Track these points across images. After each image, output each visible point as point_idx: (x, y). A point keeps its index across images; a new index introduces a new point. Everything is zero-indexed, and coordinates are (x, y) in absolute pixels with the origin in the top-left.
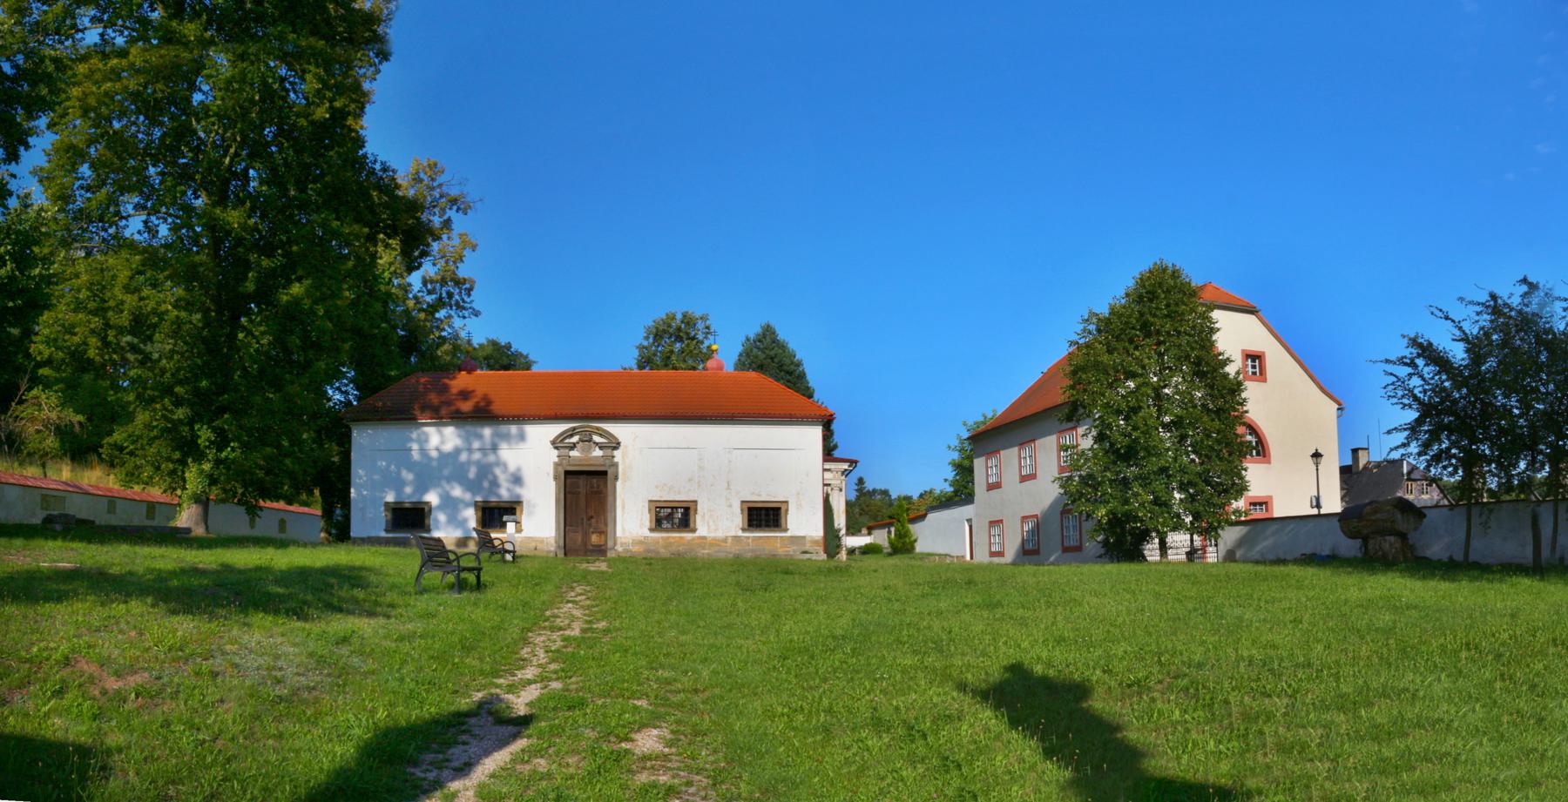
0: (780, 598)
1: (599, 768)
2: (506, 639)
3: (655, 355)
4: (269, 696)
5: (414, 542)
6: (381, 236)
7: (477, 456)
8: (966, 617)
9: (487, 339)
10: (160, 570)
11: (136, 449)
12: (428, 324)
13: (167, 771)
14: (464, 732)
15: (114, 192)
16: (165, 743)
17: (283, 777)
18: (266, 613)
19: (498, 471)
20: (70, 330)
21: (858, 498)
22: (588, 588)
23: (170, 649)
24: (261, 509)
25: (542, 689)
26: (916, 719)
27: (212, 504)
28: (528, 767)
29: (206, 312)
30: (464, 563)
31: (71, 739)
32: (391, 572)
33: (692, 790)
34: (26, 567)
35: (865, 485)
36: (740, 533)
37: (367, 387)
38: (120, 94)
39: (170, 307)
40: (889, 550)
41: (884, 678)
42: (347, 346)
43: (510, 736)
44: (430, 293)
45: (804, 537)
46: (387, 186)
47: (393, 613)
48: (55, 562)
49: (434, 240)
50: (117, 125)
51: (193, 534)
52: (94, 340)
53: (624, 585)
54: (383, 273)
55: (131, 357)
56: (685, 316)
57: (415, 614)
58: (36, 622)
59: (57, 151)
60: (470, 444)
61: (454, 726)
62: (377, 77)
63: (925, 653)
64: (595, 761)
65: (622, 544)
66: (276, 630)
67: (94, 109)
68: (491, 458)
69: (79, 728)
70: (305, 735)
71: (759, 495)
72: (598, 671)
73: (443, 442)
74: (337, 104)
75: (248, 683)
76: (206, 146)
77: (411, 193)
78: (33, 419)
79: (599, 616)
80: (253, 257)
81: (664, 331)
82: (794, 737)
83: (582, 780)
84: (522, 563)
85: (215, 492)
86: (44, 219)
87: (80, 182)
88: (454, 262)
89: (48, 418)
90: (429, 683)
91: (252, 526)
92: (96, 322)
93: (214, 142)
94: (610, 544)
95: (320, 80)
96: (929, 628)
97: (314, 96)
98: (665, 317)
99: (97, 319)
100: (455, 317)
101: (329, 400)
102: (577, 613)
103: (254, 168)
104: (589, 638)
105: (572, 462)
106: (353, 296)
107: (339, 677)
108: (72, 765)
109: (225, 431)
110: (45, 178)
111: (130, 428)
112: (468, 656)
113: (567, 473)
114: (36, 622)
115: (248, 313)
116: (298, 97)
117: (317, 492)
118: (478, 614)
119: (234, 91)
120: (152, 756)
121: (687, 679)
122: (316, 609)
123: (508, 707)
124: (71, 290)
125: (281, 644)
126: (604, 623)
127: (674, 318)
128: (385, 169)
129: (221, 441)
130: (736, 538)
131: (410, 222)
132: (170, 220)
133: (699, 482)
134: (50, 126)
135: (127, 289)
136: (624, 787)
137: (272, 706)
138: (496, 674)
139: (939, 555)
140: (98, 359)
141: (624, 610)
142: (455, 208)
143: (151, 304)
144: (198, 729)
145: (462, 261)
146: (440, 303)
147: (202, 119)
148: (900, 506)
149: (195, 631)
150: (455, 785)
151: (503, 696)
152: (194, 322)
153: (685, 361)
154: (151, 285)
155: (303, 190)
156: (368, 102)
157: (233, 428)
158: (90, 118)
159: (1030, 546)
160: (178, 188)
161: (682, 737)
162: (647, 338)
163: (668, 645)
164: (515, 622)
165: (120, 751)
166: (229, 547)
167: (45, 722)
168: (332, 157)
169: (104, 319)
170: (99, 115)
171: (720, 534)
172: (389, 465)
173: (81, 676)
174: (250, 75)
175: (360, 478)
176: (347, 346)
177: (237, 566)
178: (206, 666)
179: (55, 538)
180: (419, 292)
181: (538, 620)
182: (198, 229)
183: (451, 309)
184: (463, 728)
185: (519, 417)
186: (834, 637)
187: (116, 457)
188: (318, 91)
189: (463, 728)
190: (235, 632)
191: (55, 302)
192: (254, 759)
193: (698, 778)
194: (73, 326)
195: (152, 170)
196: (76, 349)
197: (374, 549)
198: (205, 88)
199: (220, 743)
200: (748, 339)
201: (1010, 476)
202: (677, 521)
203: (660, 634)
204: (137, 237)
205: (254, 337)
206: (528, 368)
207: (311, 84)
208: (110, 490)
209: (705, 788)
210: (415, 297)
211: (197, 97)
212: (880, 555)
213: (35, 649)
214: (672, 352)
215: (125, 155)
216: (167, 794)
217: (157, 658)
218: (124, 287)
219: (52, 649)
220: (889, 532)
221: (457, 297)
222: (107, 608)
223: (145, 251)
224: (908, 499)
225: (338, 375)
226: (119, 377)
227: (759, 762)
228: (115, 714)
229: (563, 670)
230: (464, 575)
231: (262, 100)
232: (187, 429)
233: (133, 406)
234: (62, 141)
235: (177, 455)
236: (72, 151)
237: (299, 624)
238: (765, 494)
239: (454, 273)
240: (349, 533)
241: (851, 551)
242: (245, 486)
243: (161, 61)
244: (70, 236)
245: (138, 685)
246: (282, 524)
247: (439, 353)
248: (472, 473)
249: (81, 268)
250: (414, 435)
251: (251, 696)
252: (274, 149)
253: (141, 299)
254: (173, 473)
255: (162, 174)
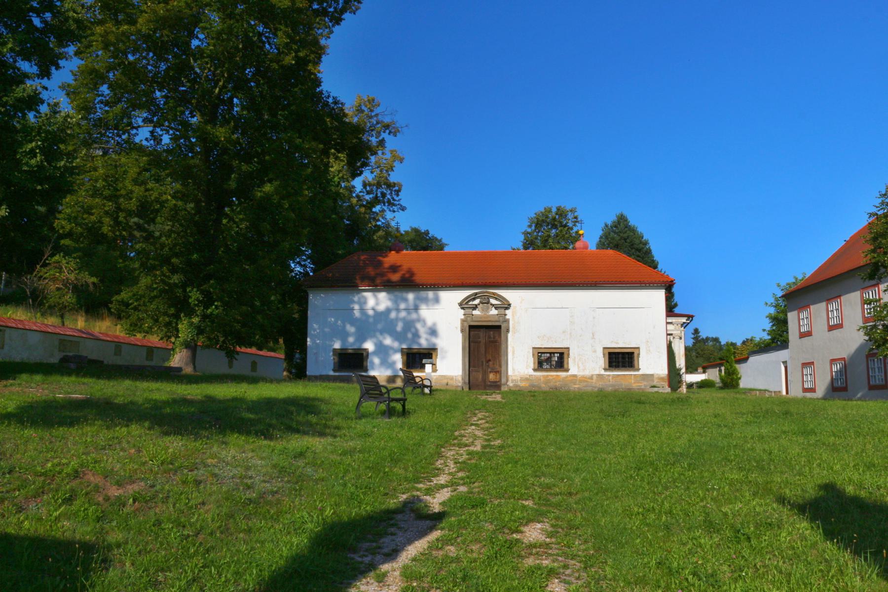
0: (635, 422)
1: (496, 553)
2: (425, 453)
3: (536, 238)
4: (241, 499)
5: (355, 379)
6: (333, 151)
7: (403, 314)
8: (784, 442)
9: (411, 227)
10: (156, 400)
11: (139, 305)
12: (367, 216)
13: (157, 562)
14: (392, 526)
15: (127, 108)
16: (156, 539)
17: (251, 563)
18: (240, 434)
19: (419, 326)
20: (88, 211)
21: (694, 344)
22: (487, 414)
23: (162, 463)
24: (238, 353)
25: (452, 491)
26: (742, 524)
27: (199, 349)
28: (441, 553)
29: (198, 202)
30: (393, 395)
31: (78, 538)
32: (338, 402)
33: (568, 572)
34: (44, 398)
35: (700, 334)
36: (603, 372)
37: (320, 262)
38: (135, 35)
39: (169, 198)
40: (721, 385)
41: (714, 488)
42: (306, 231)
43: (428, 528)
44: (368, 193)
45: (652, 375)
46: (336, 113)
47: (339, 433)
48: (69, 393)
49: (372, 155)
50: (131, 58)
51: (184, 372)
52: (108, 219)
53: (514, 412)
54: (334, 177)
55: (137, 234)
56: (558, 209)
57: (355, 434)
58: (51, 442)
59: (82, 72)
60: (398, 305)
61: (385, 521)
62: (331, 36)
63: (749, 470)
64: (493, 548)
65: (513, 381)
66: (247, 447)
67: (114, 45)
68: (414, 316)
69: (85, 529)
70: (269, 529)
71: (617, 343)
72: (495, 478)
73: (377, 304)
74: (301, 54)
75: (224, 489)
76: (201, 79)
77: (355, 120)
78: (54, 279)
79: (495, 435)
80: (235, 163)
81: (543, 221)
82: (648, 531)
83: (483, 562)
84: (437, 395)
85: (201, 341)
86: (69, 123)
87: (100, 98)
88: (387, 171)
89: (67, 279)
90: (366, 488)
91: (230, 366)
92: (109, 206)
93: (207, 76)
94: (503, 380)
95: (288, 36)
96: (753, 449)
97: (283, 47)
98: (543, 210)
99: (110, 204)
100: (388, 211)
101: (292, 271)
102: (479, 433)
103: (237, 98)
104: (488, 452)
105: (474, 319)
106: (310, 195)
107: (297, 483)
108: (78, 559)
109: (211, 293)
110: (71, 92)
111: (135, 289)
112: (396, 467)
113: (471, 327)
114: (51, 442)
115: (231, 204)
116: (272, 48)
117: (281, 341)
118: (404, 434)
119: (223, 40)
120: (146, 550)
121: (563, 484)
122: (279, 431)
123: (426, 506)
124: (90, 180)
125: (251, 458)
126: (499, 441)
127: (550, 211)
128: (336, 102)
129: (208, 301)
130: (599, 376)
131: (354, 141)
132: (171, 132)
133: (571, 334)
134: (77, 53)
135: (135, 182)
136: (515, 569)
137: (243, 507)
138: (417, 480)
139: (760, 390)
140: (110, 234)
141: (515, 431)
142: (387, 131)
143: (155, 195)
144: (184, 527)
145: (392, 170)
146: (376, 201)
147: (198, 58)
148: (729, 350)
149: (183, 449)
150: (385, 567)
151: (422, 497)
152: (189, 209)
153: (559, 243)
154: (155, 180)
155: (274, 115)
156: (324, 54)
157: (217, 291)
158: (110, 51)
159: (839, 384)
160: (178, 109)
161: (560, 530)
162: (530, 226)
163: (549, 459)
164: (432, 440)
165: (118, 546)
166: (211, 382)
167: (56, 524)
168: (296, 92)
169: (116, 203)
170: (116, 49)
171: (587, 373)
172: (336, 322)
173: (88, 486)
174: (235, 30)
175: (315, 330)
176: (306, 231)
177: (218, 397)
178: (191, 476)
179: (69, 374)
180: (360, 192)
181: (449, 439)
182: (194, 140)
183: (384, 205)
184: (392, 522)
185: (434, 285)
186: (674, 454)
187: (123, 311)
188: (287, 44)
189: (392, 522)
190: (215, 449)
191: (76, 188)
192: (228, 549)
193: (573, 562)
194: (91, 208)
195: (158, 94)
196: (93, 226)
197: (325, 384)
198: (201, 36)
199: (201, 537)
200: (606, 226)
201: (820, 328)
202: (554, 363)
203: (543, 450)
204: (145, 143)
205: (235, 223)
206: (442, 249)
207: (281, 39)
208: (117, 337)
209: (578, 571)
210: (358, 196)
211: (195, 43)
212: (713, 389)
213: (49, 465)
214: (549, 236)
215: (137, 81)
216: (157, 579)
217: (152, 470)
218: (133, 180)
219: (64, 465)
220: (720, 371)
221: (389, 196)
222: (112, 431)
223: (150, 154)
224: (733, 345)
225: (300, 253)
226: (127, 249)
227: (620, 551)
228: (115, 516)
229: (468, 477)
230: (393, 404)
231: (245, 48)
232: (180, 291)
233: (137, 272)
234: (86, 66)
235: (172, 311)
236: (94, 74)
237: (265, 442)
238: (622, 343)
239: (386, 179)
240: (306, 372)
241: (690, 386)
242: (226, 336)
243: (168, 14)
244: (90, 138)
245: (135, 492)
246: (254, 365)
247: (375, 238)
248: (399, 327)
249: (99, 163)
250: (356, 299)
251: (227, 499)
252: (252, 84)
253: (147, 190)
254: (168, 324)
255: (166, 97)
